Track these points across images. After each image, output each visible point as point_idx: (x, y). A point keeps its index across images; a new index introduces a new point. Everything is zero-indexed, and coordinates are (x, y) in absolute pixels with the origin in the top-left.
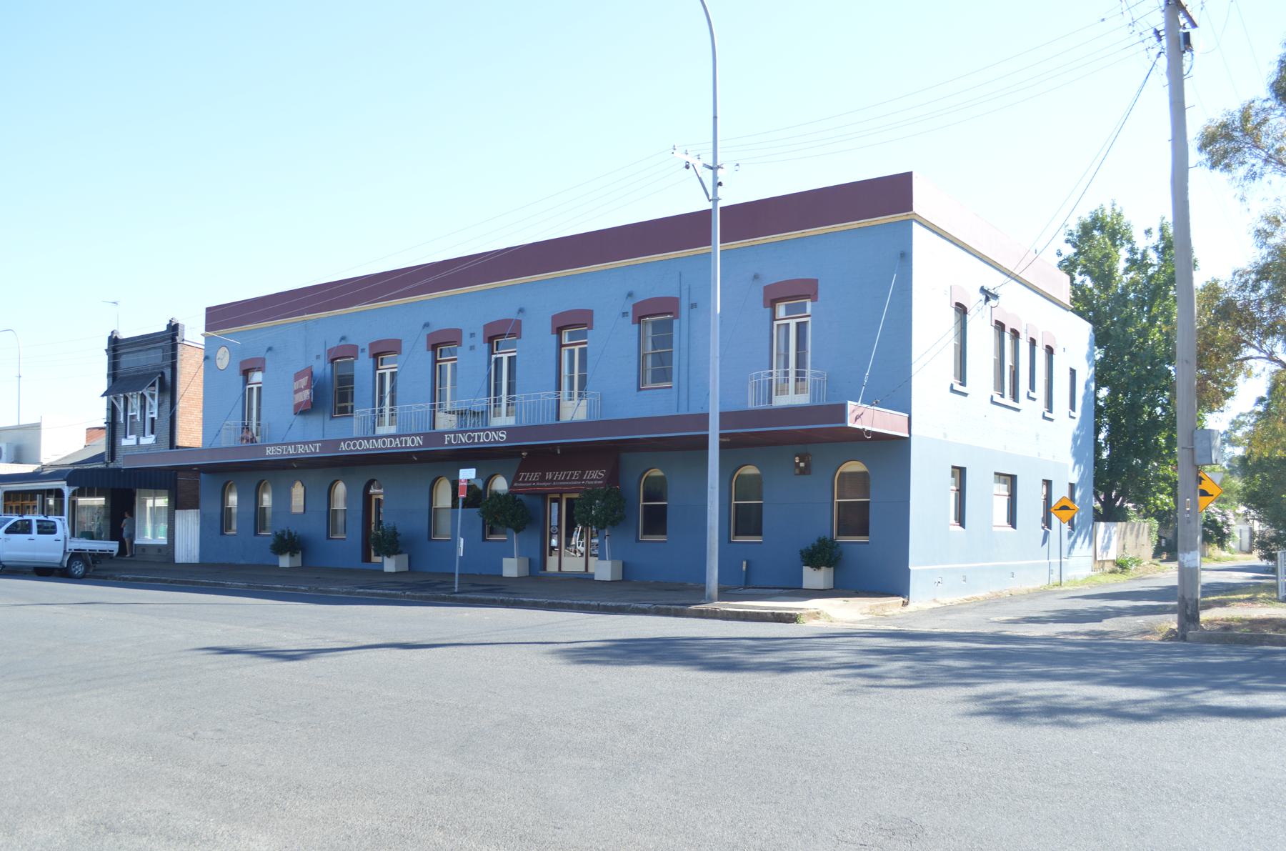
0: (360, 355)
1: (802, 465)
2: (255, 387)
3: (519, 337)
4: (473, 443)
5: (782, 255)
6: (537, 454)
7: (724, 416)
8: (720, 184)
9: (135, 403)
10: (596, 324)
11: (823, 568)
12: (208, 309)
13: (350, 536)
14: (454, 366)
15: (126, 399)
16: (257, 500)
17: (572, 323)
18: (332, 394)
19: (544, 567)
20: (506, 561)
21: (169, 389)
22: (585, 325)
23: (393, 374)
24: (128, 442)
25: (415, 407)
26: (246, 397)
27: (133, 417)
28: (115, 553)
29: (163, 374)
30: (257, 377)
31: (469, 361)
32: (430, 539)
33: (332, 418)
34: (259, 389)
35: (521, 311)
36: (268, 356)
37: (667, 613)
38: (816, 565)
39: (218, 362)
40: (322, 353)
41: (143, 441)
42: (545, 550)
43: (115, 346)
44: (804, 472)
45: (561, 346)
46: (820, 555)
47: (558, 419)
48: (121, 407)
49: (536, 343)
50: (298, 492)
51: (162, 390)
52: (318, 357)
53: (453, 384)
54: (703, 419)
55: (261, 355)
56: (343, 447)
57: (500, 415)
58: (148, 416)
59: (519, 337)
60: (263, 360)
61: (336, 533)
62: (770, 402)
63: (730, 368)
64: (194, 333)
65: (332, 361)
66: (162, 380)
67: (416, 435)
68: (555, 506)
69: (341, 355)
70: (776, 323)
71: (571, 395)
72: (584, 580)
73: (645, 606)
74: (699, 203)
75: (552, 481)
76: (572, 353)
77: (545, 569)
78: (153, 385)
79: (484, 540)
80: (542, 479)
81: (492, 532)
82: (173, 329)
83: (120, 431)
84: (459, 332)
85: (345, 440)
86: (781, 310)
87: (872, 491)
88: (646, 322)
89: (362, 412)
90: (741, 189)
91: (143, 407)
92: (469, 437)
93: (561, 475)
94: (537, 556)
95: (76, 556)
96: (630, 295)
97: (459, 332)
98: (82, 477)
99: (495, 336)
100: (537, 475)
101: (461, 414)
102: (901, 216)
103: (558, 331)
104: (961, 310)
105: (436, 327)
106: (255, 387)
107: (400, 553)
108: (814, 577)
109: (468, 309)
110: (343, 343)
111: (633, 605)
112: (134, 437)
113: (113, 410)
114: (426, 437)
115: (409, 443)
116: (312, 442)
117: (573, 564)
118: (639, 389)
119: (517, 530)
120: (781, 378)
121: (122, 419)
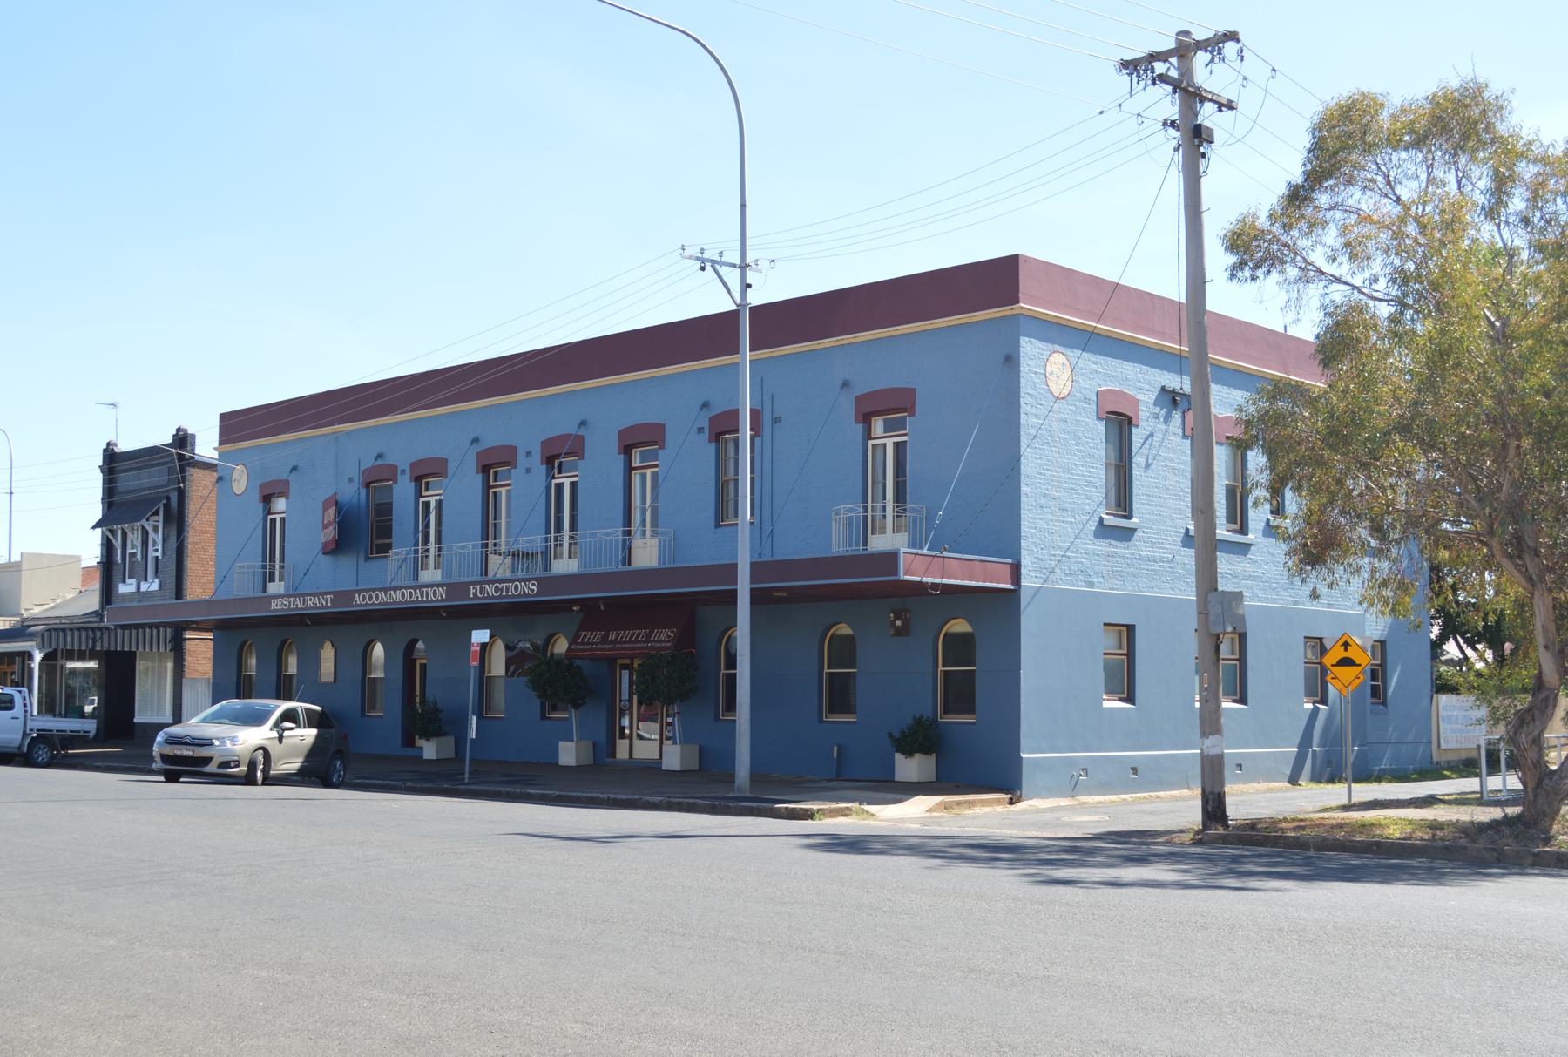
0: (400, 477)
1: (898, 623)
2: (278, 517)
3: (582, 458)
4: (501, 597)
5: (870, 357)
6: (612, 608)
7: (757, 569)
8: (749, 286)
9: (135, 538)
10: (918, 409)
11: (918, 756)
12: (224, 417)
13: (388, 710)
14: (508, 492)
15: (124, 534)
16: (280, 664)
17: (639, 441)
18: (362, 529)
19: (613, 753)
20: (562, 745)
21: (176, 519)
22: (655, 443)
23: (574, 485)
24: (126, 588)
25: (464, 546)
26: (269, 528)
27: (133, 555)
28: (92, 735)
29: (168, 498)
30: (280, 504)
31: (523, 488)
32: (363, 715)
33: (367, 559)
34: (283, 520)
35: (583, 423)
36: (292, 478)
37: (670, 807)
38: (909, 753)
39: (235, 485)
40: (355, 473)
41: (144, 587)
42: (613, 733)
43: (113, 461)
44: (900, 632)
45: (629, 469)
46: (920, 738)
47: (179, 594)
48: (118, 544)
49: (598, 468)
50: (328, 653)
51: (167, 521)
52: (351, 480)
53: (508, 516)
54: (732, 569)
55: (284, 477)
56: (358, 599)
57: (883, 530)
58: (152, 554)
59: (582, 458)
60: (287, 482)
61: (374, 708)
62: (865, 543)
63: (801, 498)
64: (207, 446)
65: (368, 485)
66: (167, 507)
67: (438, 585)
68: (626, 674)
69: (377, 479)
70: (871, 442)
71: (644, 533)
72: (652, 768)
73: (657, 799)
74: (721, 304)
75: (615, 642)
76: (643, 476)
77: (614, 755)
78: (156, 513)
79: (543, 717)
80: (605, 640)
81: (554, 708)
82: (183, 439)
83: (117, 575)
84: (512, 450)
85: (360, 592)
86: (878, 425)
87: (979, 656)
88: (726, 441)
89: (400, 551)
90: (774, 286)
91: (145, 543)
92: (497, 589)
93: (625, 635)
94: (602, 737)
95: (44, 738)
96: (705, 405)
97: (512, 450)
98: (61, 638)
99: (556, 455)
100: (599, 634)
101: (515, 555)
102: (1005, 311)
103: (627, 450)
104: (1120, 424)
105: (862, 389)
106: (278, 517)
107: (444, 735)
108: (909, 767)
109: (523, 420)
110: (379, 462)
111: (645, 798)
112: (134, 581)
113: (108, 546)
114: (540, 581)
115: (431, 596)
116: (323, 594)
117: (646, 750)
118: (718, 526)
119: (576, 707)
120: (879, 514)
121: (119, 558)
